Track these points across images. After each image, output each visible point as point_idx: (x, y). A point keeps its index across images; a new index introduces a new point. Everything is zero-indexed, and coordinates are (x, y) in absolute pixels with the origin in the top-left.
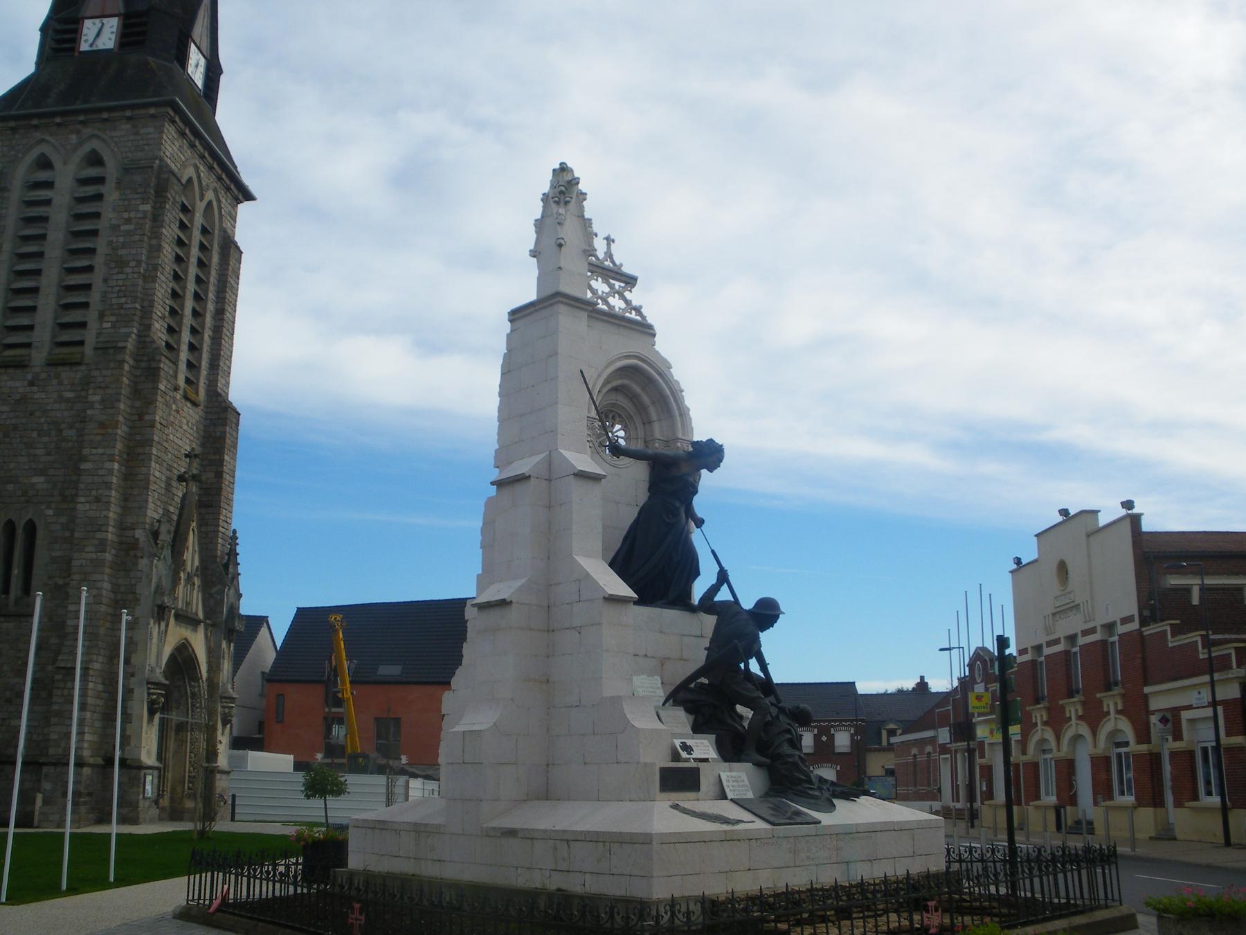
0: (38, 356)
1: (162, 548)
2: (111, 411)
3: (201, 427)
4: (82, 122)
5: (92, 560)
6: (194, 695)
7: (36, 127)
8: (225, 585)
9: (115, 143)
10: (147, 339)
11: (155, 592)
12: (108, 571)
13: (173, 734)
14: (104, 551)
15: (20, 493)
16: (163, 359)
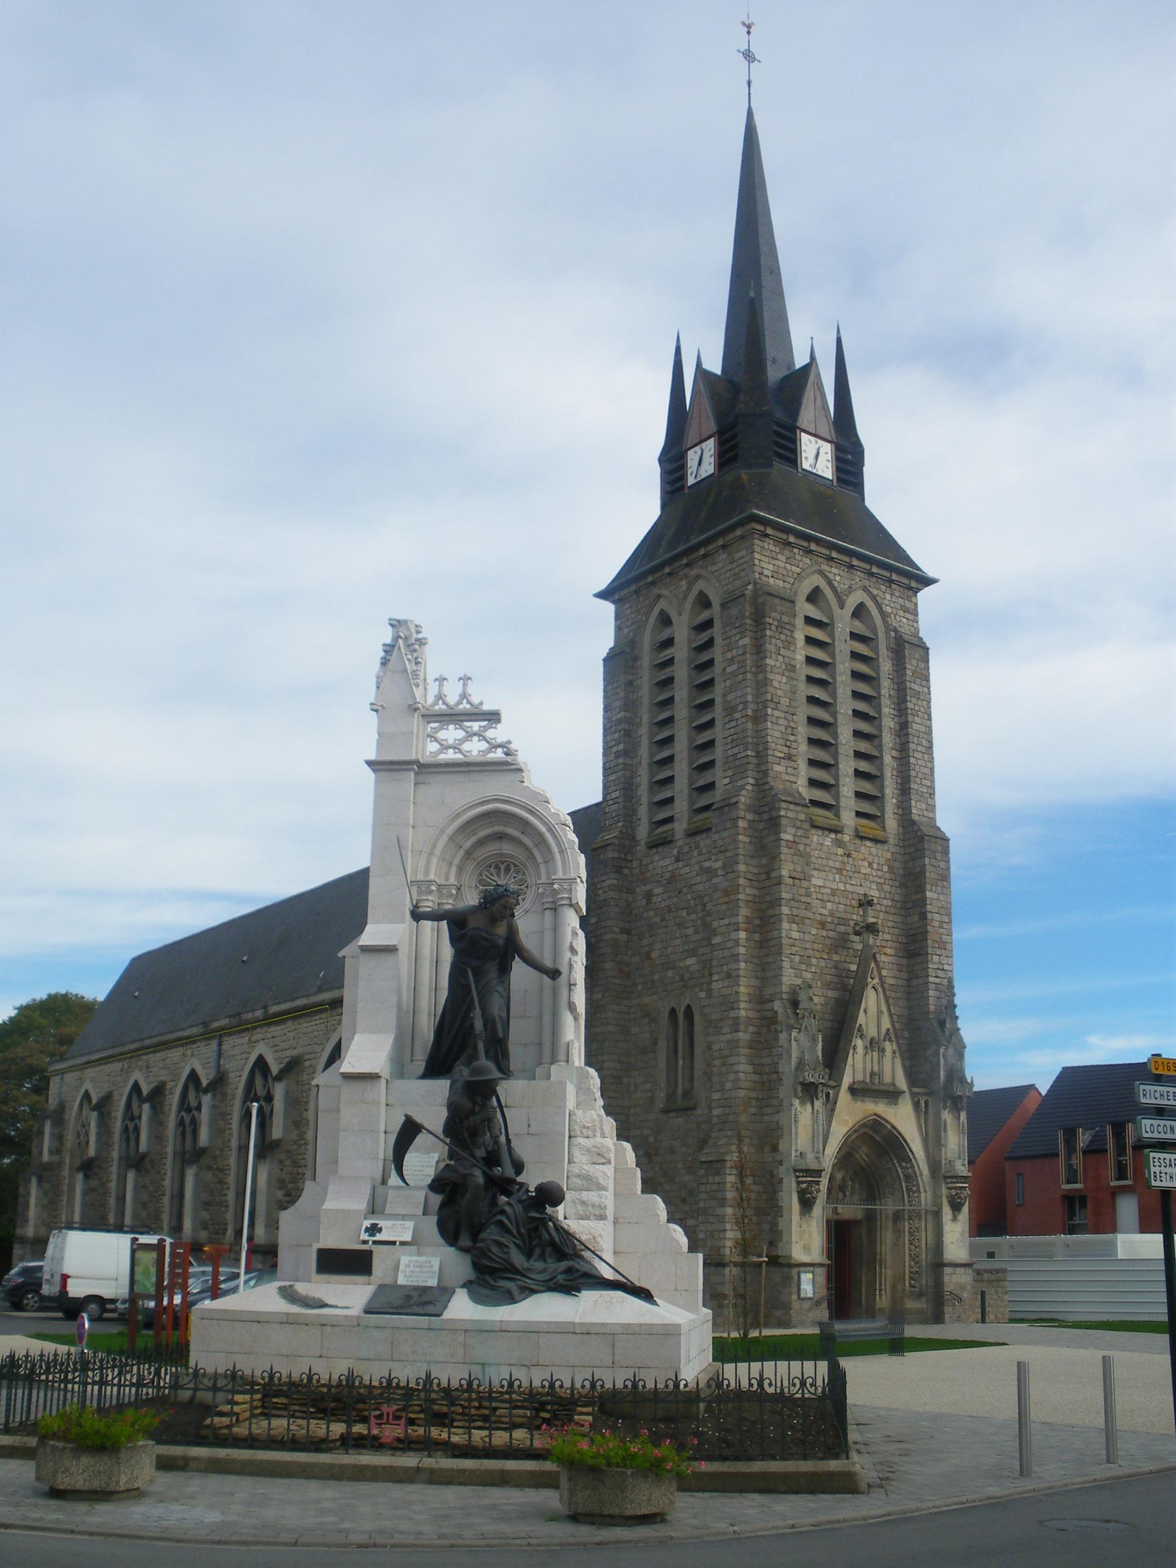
0: (679, 828)
2: (731, 876)
3: (897, 865)
4: (687, 565)
5: (729, 1042)
6: (908, 1178)
7: (653, 583)
8: (939, 1045)
9: (713, 580)
10: (767, 787)
11: (797, 1069)
12: (746, 1051)
13: (891, 1225)
15: (677, 978)
16: (784, 805)
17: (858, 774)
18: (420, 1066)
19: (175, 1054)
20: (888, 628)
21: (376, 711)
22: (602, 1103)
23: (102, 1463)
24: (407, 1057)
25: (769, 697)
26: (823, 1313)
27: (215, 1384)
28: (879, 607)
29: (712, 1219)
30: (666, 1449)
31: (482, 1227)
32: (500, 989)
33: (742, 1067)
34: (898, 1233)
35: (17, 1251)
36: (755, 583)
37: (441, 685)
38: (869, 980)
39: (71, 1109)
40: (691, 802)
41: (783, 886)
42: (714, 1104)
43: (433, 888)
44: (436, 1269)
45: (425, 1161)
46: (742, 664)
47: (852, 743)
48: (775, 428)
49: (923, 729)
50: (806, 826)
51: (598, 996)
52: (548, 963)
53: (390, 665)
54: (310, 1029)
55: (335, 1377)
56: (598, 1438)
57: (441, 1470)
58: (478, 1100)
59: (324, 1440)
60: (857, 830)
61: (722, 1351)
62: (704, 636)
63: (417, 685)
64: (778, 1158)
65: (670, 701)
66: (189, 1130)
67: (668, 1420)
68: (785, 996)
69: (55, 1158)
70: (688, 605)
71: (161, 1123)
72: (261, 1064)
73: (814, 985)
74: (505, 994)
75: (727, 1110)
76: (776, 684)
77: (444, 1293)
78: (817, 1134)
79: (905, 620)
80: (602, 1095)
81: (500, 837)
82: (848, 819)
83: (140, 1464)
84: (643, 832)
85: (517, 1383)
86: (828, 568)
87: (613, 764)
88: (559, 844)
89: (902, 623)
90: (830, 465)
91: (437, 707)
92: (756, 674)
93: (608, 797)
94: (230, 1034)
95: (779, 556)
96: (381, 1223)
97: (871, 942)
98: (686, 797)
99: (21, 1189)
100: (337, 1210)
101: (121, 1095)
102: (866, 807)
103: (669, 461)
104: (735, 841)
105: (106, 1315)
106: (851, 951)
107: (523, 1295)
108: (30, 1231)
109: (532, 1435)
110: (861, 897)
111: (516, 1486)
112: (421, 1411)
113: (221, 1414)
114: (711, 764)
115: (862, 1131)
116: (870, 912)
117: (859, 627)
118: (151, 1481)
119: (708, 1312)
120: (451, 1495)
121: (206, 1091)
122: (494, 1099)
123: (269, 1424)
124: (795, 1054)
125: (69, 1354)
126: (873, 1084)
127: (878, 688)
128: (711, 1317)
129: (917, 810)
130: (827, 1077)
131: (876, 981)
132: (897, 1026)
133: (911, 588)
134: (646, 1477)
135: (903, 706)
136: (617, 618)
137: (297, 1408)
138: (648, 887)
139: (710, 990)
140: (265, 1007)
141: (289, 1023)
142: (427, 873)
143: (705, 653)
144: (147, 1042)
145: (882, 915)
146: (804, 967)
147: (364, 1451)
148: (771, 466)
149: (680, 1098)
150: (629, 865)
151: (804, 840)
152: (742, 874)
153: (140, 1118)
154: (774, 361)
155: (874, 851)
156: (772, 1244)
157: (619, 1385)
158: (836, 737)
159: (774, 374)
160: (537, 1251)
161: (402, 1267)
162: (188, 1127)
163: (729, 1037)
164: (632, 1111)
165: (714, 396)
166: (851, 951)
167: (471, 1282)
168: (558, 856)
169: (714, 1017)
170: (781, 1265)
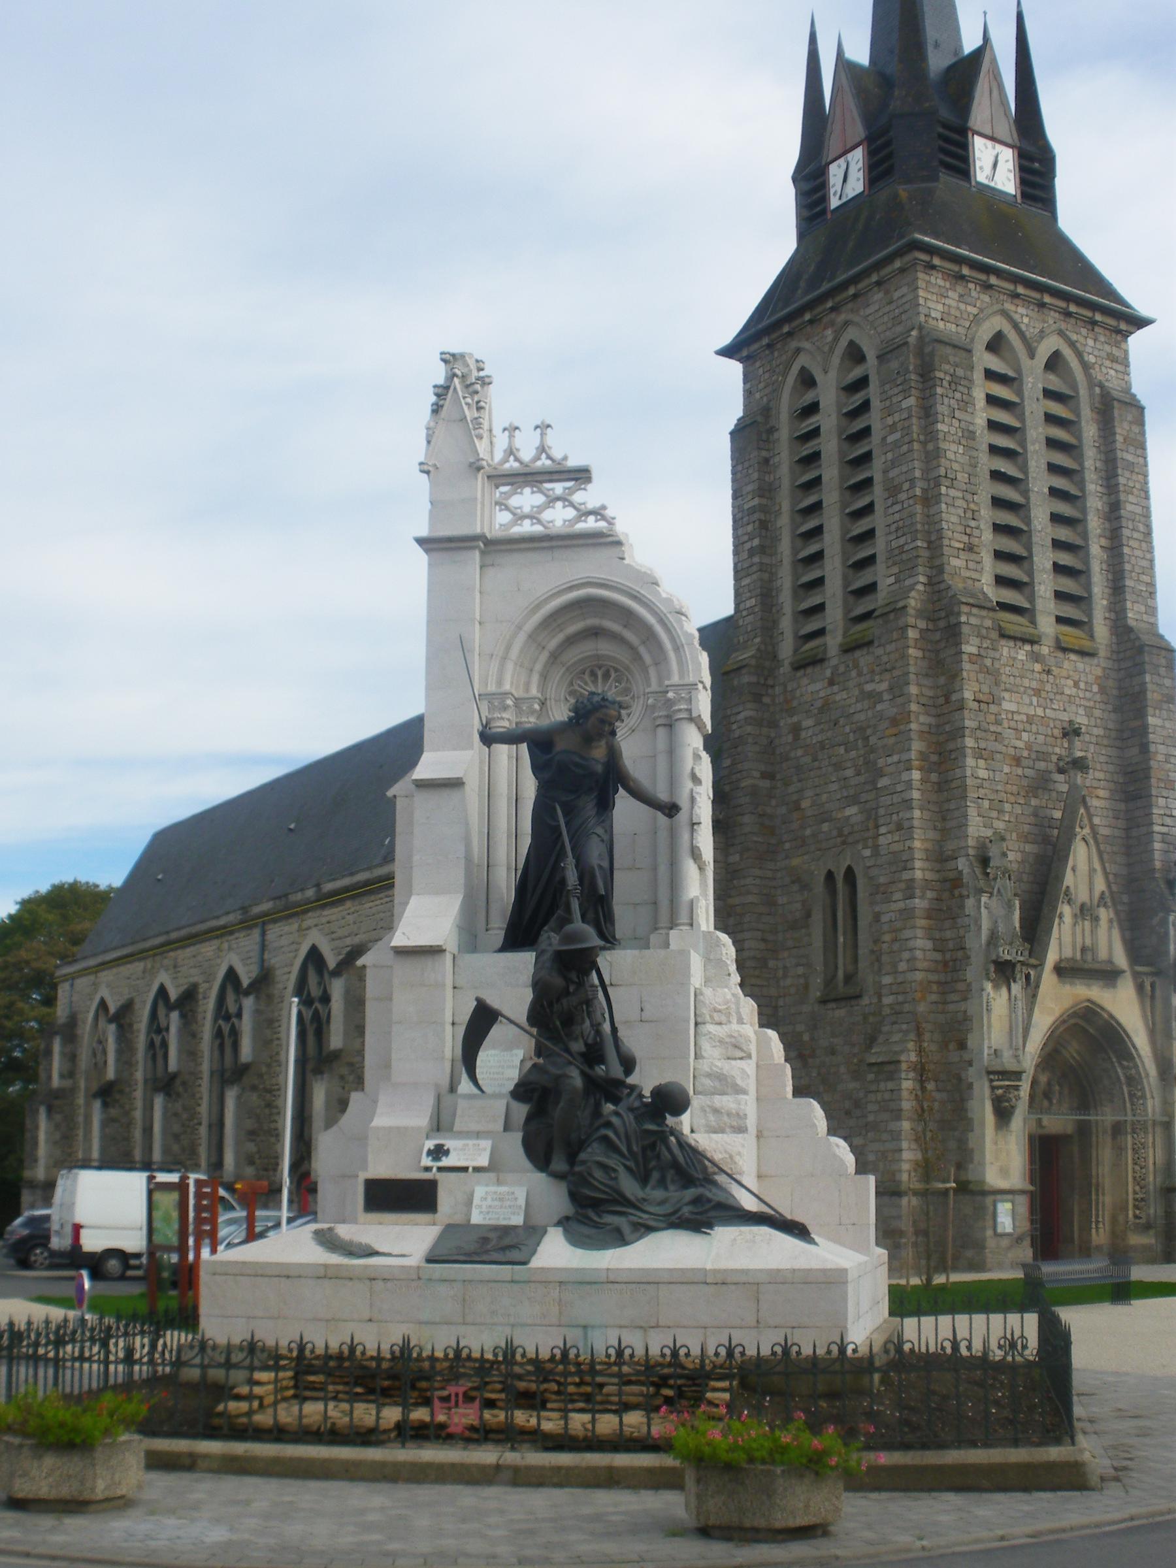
0: (833, 642)
1: (995, 879)
2: (900, 700)
3: (1111, 683)
4: (832, 309)
5: (901, 911)
10: (942, 586)
11: (989, 944)
13: (1109, 1139)
14: (912, 897)
15: (835, 833)
16: (965, 609)
17: (1058, 569)
18: (498, 935)
19: (207, 949)
20: (1092, 382)
21: (428, 472)
22: (739, 979)
23: (73, 1464)
24: (481, 923)
25: (942, 472)
26: (1026, 1253)
27: (228, 1360)
28: (1079, 355)
29: (885, 1136)
30: (830, 1437)
31: (582, 1145)
32: (600, 830)
33: (919, 943)
34: (1119, 1150)
35: (26, 1197)
36: (921, 328)
37: (511, 437)
38: (1078, 830)
39: (84, 1022)
40: (847, 610)
41: (966, 712)
42: (884, 991)
43: (509, 702)
44: (522, 1202)
45: (505, 1060)
46: (907, 431)
47: (1049, 530)
48: (941, 130)
49: (1138, 510)
50: (994, 635)
51: (735, 858)
52: (663, 796)
53: (444, 413)
54: (374, 910)
55: (385, 1348)
56: (736, 1425)
57: (529, 1468)
58: (573, 976)
59: (372, 1431)
60: (1058, 640)
61: (901, 1302)
62: (857, 399)
63: (480, 437)
64: (966, 1057)
65: (816, 482)
66: (228, 1043)
67: (832, 1395)
68: (971, 852)
69: (68, 1083)
70: (836, 360)
71: (194, 1035)
72: (314, 956)
73: (1008, 837)
74: (606, 837)
75: (900, 998)
76: (950, 455)
77: (532, 1233)
78: (1014, 1026)
79: (1112, 372)
80: (738, 969)
81: (595, 633)
82: (1046, 625)
83: (125, 1465)
84: (786, 649)
85: (628, 1352)
86: (1013, 308)
87: (746, 565)
88: (673, 639)
89: (1108, 375)
90: (1012, 176)
91: (507, 466)
92: (924, 444)
93: (742, 606)
94: (275, 921)
95: (950, 293)
96: (449, 1144)
97: (1079, 781)
98: (840, 603)
99: (28, 1122)
100: (390, 1128)
101: (144, 1002)
102: (1069, 611)
103: (807, 178)
104: (904, 656)
105: (130, 1273)
106: (1054, 794)
107: (639, 1234)
108: (40, 1173)
109: (649, 1419)
110: (1066, 725)
111: (628, 1487)
112: (501, 1391)
113: (239, 1398)
114: (870, 560)
115: (1072, 1021)
116: (1078, 743)
117: (1055, 382)
118: (140, 1487)
119: (882, 1253)
120: (540, 1501)
121: (247, 993)
122: (594, 973)
123: (301, 1410)
124: (986, 925)
125: (66, 1320)
126: (1085, 962)
127: (1079, 458)
128: (886, 1258)
129: (1133, 615)
130: (1026, 953)
131: (1087, 831)
132: (1114, 888)
133: (1119, 332)
134: (802, 1476)
135: (1113, 482)
136: (745, 381)
137: (340, 1388)
138: (795, 719)
139: (876, 847)
140: (318, 885)
141: (348, 904)
142: (500, 683)
143: (859, 420)
144: (174, 935)
145: (1092, 748)
146: (994, 814)
147: (428, 1444)
148: (936, 179)
149: (841, 984)
150: (770, 691)
151: (992, 654)
152: (914, 698)
153: (167, 1029)
154: (937, 45)
155: (1080, 666)
156: (960, 1166)
157: (766, 1351)
158: (1028, 522)
159: (937, 62)
160: (656, 1175)
161: (476, 1201)
162: (227, 1039)
163: (901, 905)
164: (781, 1003)
165: (861, 92)
166: (1054, 794)
167: (567, 1218)
168: (672, 655)
169: (882, 880)
170: (973, 1193)
